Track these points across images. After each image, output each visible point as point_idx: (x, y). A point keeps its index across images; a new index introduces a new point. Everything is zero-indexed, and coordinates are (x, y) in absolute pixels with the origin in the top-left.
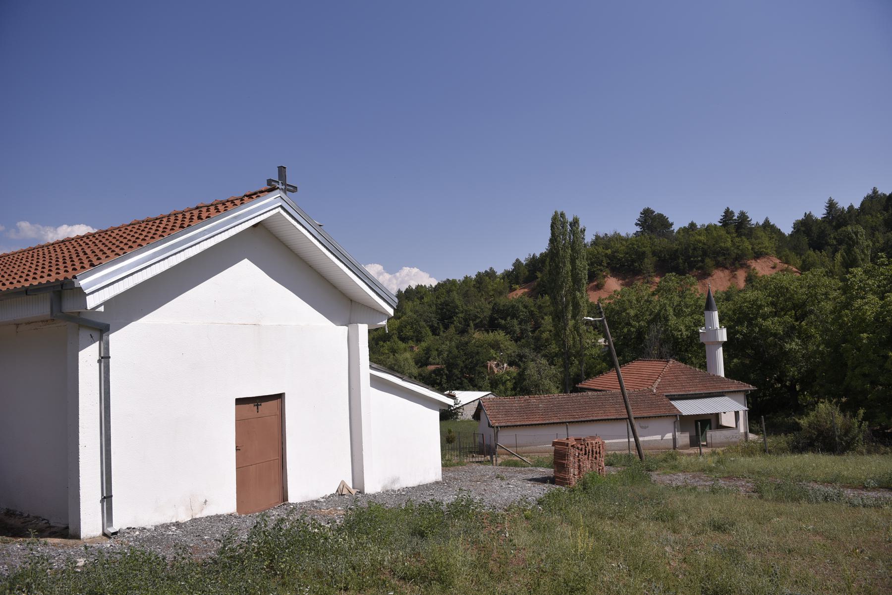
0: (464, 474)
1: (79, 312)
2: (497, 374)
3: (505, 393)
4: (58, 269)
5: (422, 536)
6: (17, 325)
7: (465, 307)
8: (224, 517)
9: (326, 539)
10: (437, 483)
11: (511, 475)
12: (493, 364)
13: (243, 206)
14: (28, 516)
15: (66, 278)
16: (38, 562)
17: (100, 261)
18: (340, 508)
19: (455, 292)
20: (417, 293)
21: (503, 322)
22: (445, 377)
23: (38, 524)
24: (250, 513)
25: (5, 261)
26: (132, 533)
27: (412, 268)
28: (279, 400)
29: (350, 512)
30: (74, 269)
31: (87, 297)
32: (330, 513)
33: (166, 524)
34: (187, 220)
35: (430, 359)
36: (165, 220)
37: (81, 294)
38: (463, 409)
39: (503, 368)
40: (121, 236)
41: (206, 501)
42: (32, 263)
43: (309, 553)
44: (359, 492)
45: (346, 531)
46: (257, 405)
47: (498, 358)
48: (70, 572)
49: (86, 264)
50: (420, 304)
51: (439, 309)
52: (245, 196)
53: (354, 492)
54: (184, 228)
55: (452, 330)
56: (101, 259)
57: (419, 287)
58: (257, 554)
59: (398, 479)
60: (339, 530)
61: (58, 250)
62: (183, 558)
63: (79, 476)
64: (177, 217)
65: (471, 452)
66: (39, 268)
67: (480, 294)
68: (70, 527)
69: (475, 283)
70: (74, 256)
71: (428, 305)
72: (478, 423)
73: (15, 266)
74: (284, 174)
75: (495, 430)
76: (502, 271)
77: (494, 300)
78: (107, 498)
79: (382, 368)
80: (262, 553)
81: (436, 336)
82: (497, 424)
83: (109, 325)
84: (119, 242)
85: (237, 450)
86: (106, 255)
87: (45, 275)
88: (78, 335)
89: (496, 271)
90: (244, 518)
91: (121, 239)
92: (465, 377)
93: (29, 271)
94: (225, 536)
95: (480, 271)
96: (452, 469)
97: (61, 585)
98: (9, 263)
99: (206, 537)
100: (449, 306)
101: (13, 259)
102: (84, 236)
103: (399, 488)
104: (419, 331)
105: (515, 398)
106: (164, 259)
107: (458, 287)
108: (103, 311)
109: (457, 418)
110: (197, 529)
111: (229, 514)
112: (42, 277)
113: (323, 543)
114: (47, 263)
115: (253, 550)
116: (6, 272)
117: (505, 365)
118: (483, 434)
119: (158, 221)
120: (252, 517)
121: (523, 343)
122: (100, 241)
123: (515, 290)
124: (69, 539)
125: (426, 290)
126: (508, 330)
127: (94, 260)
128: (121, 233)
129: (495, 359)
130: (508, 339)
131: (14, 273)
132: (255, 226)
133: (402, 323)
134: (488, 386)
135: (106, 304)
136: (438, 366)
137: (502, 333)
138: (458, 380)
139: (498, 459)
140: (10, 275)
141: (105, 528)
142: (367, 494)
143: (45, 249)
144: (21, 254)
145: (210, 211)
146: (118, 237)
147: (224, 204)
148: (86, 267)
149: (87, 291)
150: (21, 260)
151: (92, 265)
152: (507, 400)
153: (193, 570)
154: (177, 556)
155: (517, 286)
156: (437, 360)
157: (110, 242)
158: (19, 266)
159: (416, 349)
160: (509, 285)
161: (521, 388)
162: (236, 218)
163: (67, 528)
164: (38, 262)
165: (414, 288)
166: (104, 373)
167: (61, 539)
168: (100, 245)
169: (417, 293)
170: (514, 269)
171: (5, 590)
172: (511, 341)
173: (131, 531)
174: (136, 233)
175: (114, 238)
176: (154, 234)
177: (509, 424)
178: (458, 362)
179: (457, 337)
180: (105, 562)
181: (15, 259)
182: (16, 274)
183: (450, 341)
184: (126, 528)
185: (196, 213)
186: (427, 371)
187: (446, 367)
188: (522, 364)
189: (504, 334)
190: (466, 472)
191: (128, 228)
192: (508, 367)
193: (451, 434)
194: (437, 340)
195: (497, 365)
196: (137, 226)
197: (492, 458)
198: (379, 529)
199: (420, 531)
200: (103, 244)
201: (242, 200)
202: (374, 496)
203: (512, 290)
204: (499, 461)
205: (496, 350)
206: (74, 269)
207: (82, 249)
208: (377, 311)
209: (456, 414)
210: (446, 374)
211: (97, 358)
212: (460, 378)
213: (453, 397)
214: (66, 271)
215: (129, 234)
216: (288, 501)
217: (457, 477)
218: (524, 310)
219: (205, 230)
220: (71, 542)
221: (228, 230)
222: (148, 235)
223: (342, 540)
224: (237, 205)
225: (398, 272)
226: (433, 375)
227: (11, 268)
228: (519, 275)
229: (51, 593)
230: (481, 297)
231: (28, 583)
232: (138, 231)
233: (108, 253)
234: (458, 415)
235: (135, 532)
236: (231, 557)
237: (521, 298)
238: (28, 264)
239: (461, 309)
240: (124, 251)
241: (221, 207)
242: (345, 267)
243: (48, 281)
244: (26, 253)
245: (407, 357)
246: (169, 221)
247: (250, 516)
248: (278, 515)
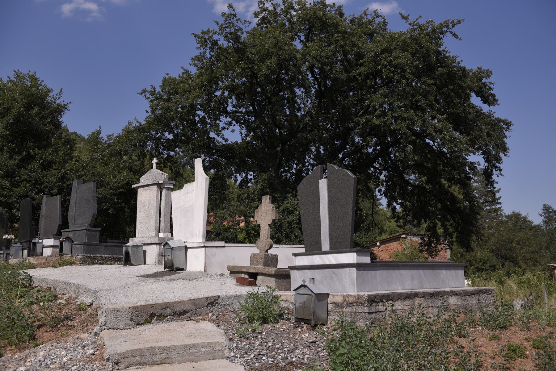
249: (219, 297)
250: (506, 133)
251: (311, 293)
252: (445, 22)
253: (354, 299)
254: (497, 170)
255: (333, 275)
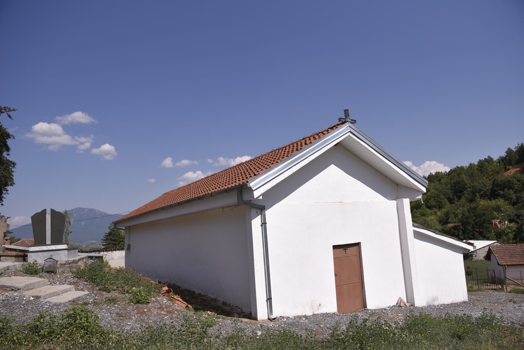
0: (484, 298)
1: (250, 200)
2: (500, 228)
3: (508, 242)
4: (239, 178)
5: (460, 339)
6: (223, 208)
7: (471, 184)
8: (331, 314)
9: (394, 334)
10: (465, 302)
11: (521, 300)
12: (497, 221)
13: (329, 134)
14: (233, 306)
15: (243, 183)
16: (239, 332)
17: (258, 173)
18: (400, 315)
19: (463, 174)
20: (436, 177)
21: (502, 192)
22: (461, 231)
23: (237, 310)
24: (345, 313)
25: (215, 177)
26: (283, 320)
27: (431, 162)
28: (358, 247)
29: (408, 318)
30: (247, 178)
31: (254, 192)
32: (394, 317)
33: (300, 316)
34: (299, 146)
35: (450, 220)
36: (288, 147)
37: (251, 190)
38: (476, 253)
39: (505, 224)
40: (267, 159)
41: (320, 304)
42: (227, 177)
43: (384, 342)
44: (412, 305)
45: (407, 330)
46: (345, 249)
47: (500, 217)
48: (253, 338)
49: (252, 175)
50: (439, 184)
51: (453, 186)
52: (329, 128)
53: (408, 305)
54: (298, 150)
55: (463, 200)
56: (259, 171)
57: (438, 174)
58: (353, 339)
59: (437, 298)
60: (402, 329)
61: (238, 169)
62: (311, 337)
63: (255, 287)
64: (294, 145)
65: (486, 282)
66: (231, 179)
67: (482, 175)
68: (252, 313)
69: (478, 167)
70: (246, 171)
71: (445, 185)
72: (489, 262)
73: (219, 179)
74: (348, 114)
75: (504, 268)
76: (498, 157)
77: (493, 178)
78: (269, 299)
79: (421, 226)
80: (355, 339)
81: (452, 204)
82: (504, 263)
83: (265, 206)
84: (266, 162)
85: (335, 275)
86: (261, 169)
87: (233, 182)
88: (251, 212)
89: (493, 158)
90: (342, 316)
91: (267, 160)
92: (476, 231)
93: (226, 181)
94: (334, 327)
95: (480, 159)
96: (474, 293)
97: (251, 345)
98: (217, 178)
99: (322, 326)
100: (460, 184)
101: (218, 176)
102: (249, 161)
103: (438, 304)
104: (440, 201)
105: (517, 245)
106: (289, 169)
107: (465, 171)
108: (262, 199)
109: (472, 259)
110: (316, 320)
111: (333, 313)
112: (232, 183)
113: (393, 336)
114: (233, 176)
115: (350, 336)
116: (216, 182)
117: (506, 222)
118: (494, 270)
119: (284, 149)
120: (347, 316)
121: (519, 206)
122: (257, 162)
123: (509, 169)
124: (252, 320)
125: (443, 175)
126: (506, 198)
127: (255, 172)
128: (266, 157)
129: (498, 218)
130: (506, 204)
131: (219, 182)
132: (336, 145)
133: (427, 197)
134: (494, 237)
135: (263, 195)
136: (455, 224)
137: (502, 200)
138: (471, 233)
139: (508, 288)
140: (218, 184)
141: (269, 315)
142: (416, 307)
143: (232, 169)
144: (221, 173)
145: (311, 140)
146: (265, 159)
147: (318, 135)
148: (252, 176)
149: (254, 189)
150: (222, 175)
151: (255, 175)
152: (511, 246)
153: (317, 345)
154: (307, 335)
155: (511, 167)
156: (455, 220)
157: (262, 162)
158: (221, 179)
159: (439, 213)
160: (504, 166)
161: (521, 238)
162: (325, 141)
163: (251, 314)
164: (229, 176)
165: (434, 174)
166: (264, 232)
167: (248, 320)
168: (257, 164)
169: (436, 177)
170: (507, 156)
171: (225, 344)
172: (510, 205)
173: (282, 318)
174: (274, 156)
175: (264, 160)
176: (283, 156)
177: (514, 263)
178: (470, 221)
179: (467, 204)
180: (271, 334)
181: (219, 175)
182: (221, 183)
183: (463, 207)
184: (279, 316)
185: (303, 141)
186: (447, 227)
187: (461, 224)
188: (519, 221)
189: (503, 201)
190: (485, 296)
191: (270, 154)
192: (509, 223)
193: (469, 270)
194: (453, 207)
195: (500, 222)
196: (274, 153)
197: (502, 287)
198: (429, 331)
199: (458, 335)
200: (259, 164)
201: (327, 131)
202: (422, 308)
203: (506, 170)
204: (509, 289)
205: (498, 212)
206: (247, 178)
207: (249, 167)
208: (415, 190)
209: (471, 256)
210: (462, 229)
211: (260, 224)
212: (472, 232)
213: (472, 244)
214: (243, 179)
215: (270, 157)
216: (367, 307)
217: (478, 299)
218: (518, 183)
219: (309, 151)
220: (253, 321)
221: (321, 149)
222: (280, 156)
223: (404, 336)
224: (325, 134)
225: (422, 164)
226: (452, 230)
227: (218, 180)
228: (511, 159)
229: (246, 349)
230: (483, 176)
231: (235, 342)
232: (275, 155)
233: (262, 168)
234: (473, 257)
235: (284, 319)
236: (338, 339)
237: (514, 175)
238: (225, 177)
239: (469, 186)
240: (269, 166)
241: (316, 137)
242: (392, 164)
243: (235, 185)
244: (223, 172)
245: (432, 219)
246: (290, 148)
247: (345, 315)
248: (362, 316)
249: (9, 266)
250: (13, 169)
251: (54, 261)
252: (5, 107)
253: (72, 261)
254: (5, 190)
255: (55, 254)
